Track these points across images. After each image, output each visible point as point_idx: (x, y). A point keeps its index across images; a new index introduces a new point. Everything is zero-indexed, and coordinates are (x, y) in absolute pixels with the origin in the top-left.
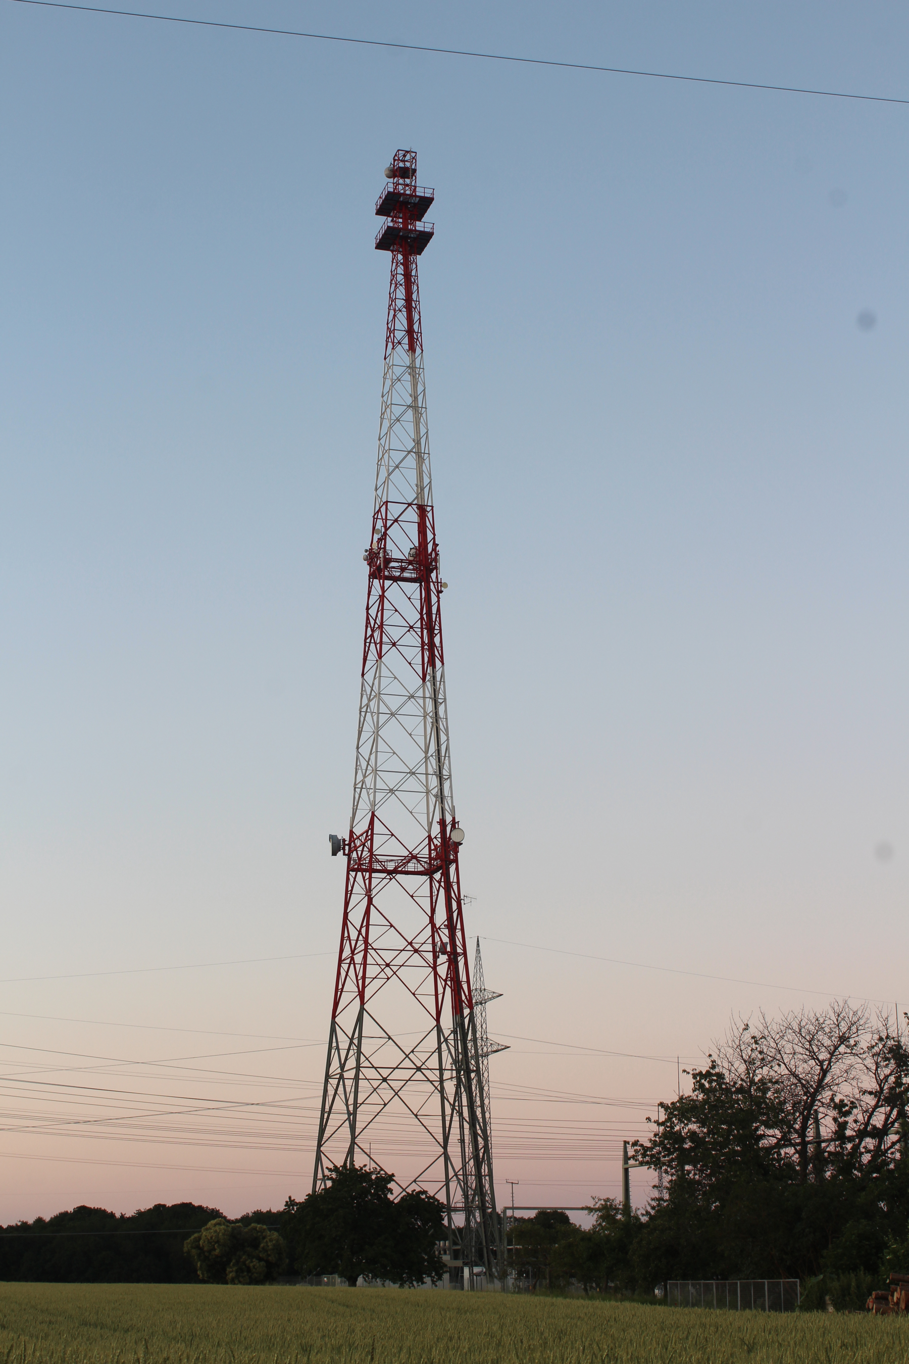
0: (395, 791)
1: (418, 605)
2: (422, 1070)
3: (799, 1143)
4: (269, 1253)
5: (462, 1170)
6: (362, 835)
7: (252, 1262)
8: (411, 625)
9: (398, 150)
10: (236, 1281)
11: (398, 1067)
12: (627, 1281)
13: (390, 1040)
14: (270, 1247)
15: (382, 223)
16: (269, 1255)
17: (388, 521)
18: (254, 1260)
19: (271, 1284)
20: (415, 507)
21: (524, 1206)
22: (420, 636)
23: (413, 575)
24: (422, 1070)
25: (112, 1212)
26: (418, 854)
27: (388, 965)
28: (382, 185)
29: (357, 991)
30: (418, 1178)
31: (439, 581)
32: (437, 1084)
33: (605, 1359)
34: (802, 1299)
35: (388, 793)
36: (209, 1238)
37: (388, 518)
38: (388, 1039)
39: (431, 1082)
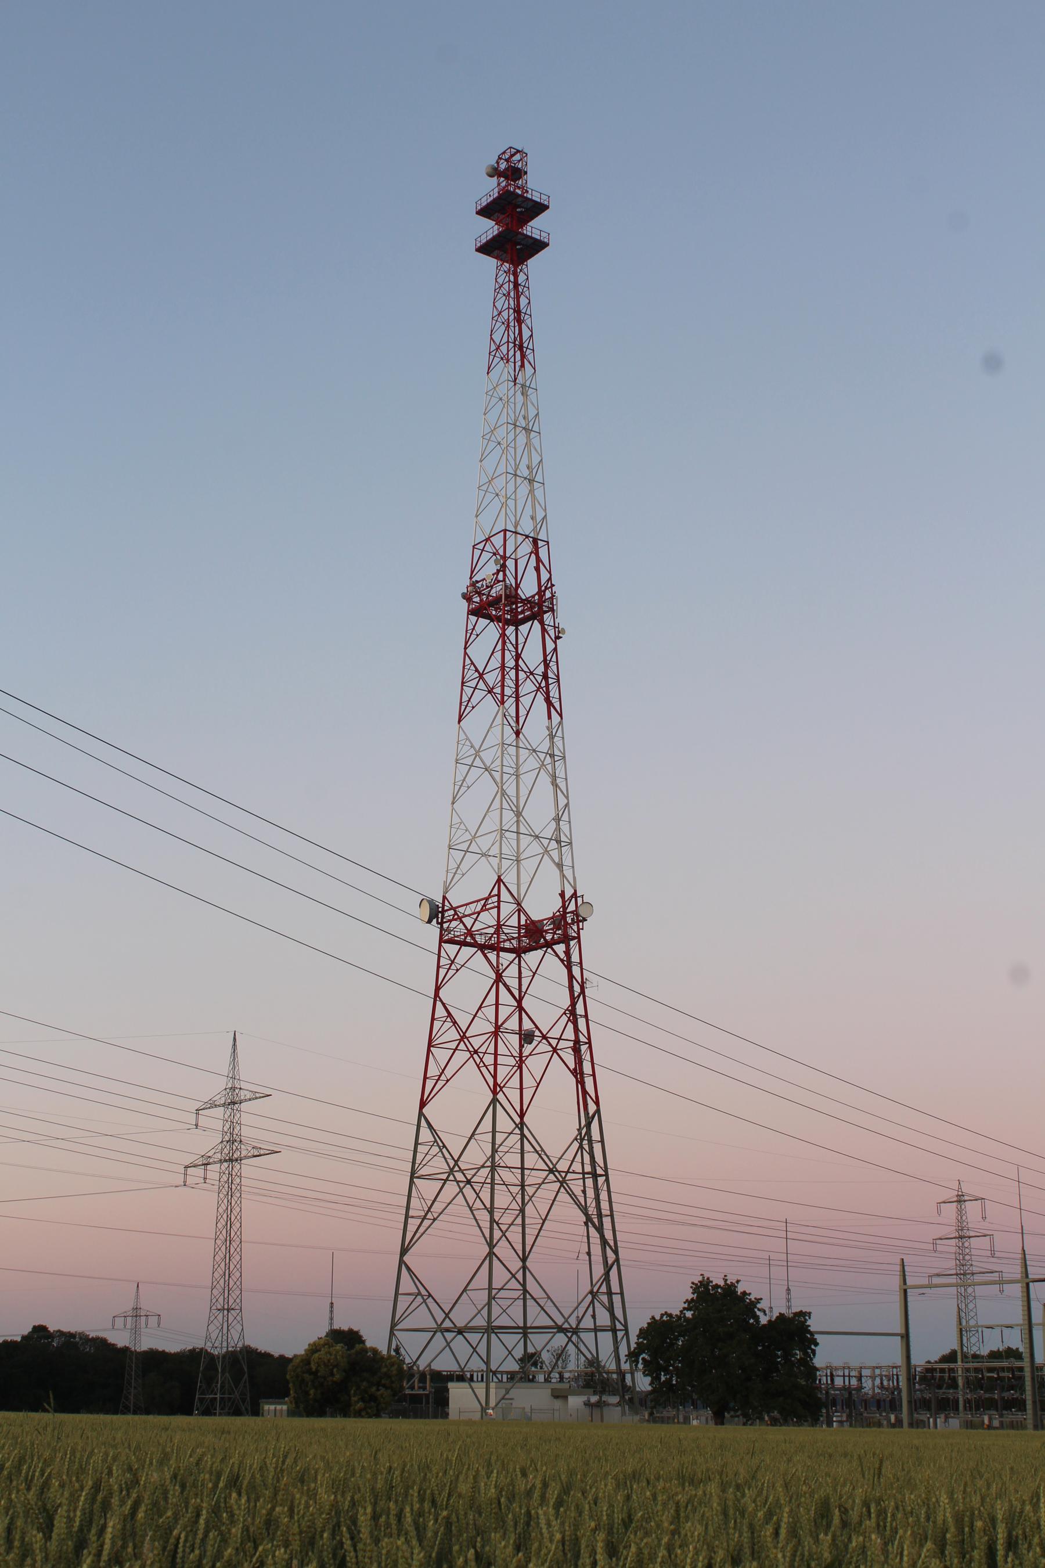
4: (393, 1379)
7: (378, 1390)
8: (489, 694)
9: (511, 148)
10: (363, 1413)
14: (395, 1372)
15: (489, 229)
16: (392, 1382)
18: (380, 1388)
19: (748, 1420)
20: (531, 539)
25: (704, 1291)
27: (476, 1052)
28: (489, 188)
29: (573, 1038)
31: (557, 625)
32: (516, 1190)
33: (531, 1465)
34: (52, 1405)
36: (326, 1361)
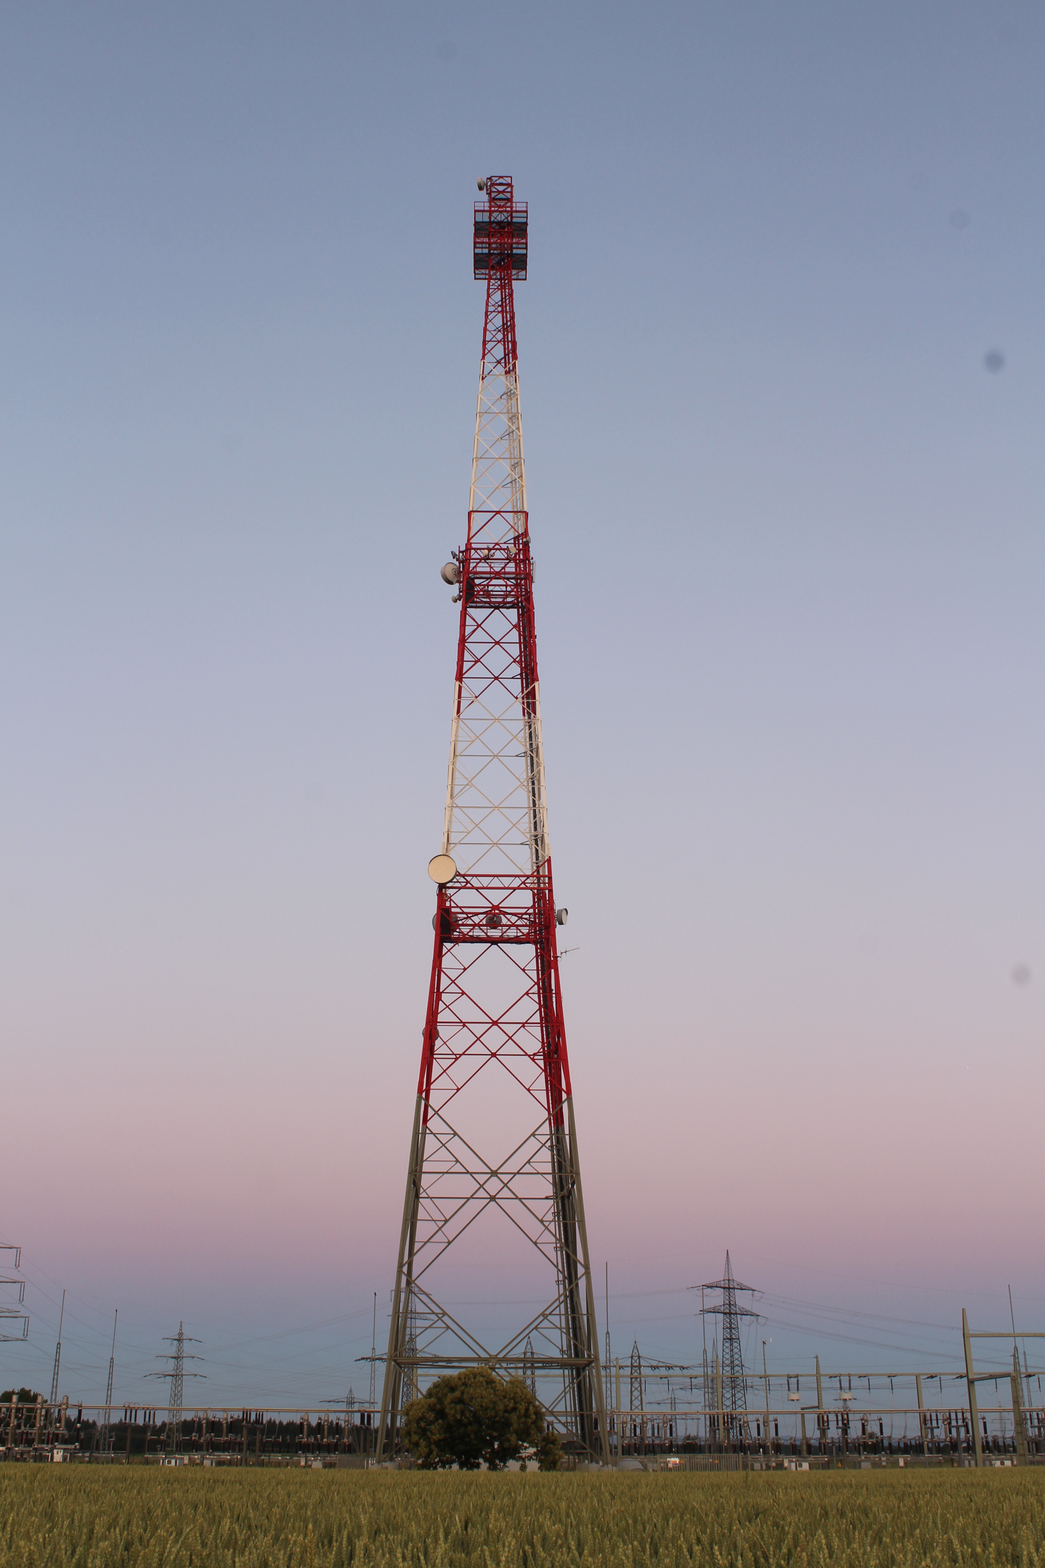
0: (494, 311)
1: (542, 1096)
2: (499, 1025)
3: (523, 564)
5: (538, 1011)
6: (487, 353)
11: (512, 1175)
12: (601, 1463)
13: (456, 1136)
17: (518, 641)
21: (538, 631)
22: (547, 1108)
23: (496, 259)
24: (499, 1025)
26: (557, 1267)
30: (541, 1324)
35: (565, 1396)
37: (518, 644)
38: (455, 1163)
39: (432, 1133)
